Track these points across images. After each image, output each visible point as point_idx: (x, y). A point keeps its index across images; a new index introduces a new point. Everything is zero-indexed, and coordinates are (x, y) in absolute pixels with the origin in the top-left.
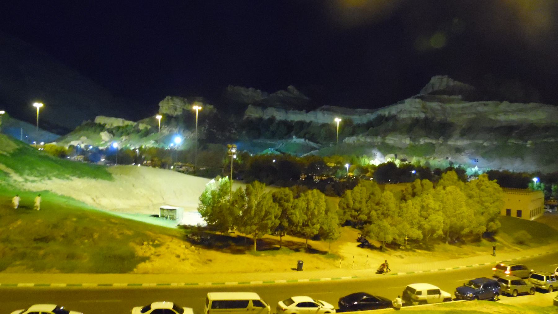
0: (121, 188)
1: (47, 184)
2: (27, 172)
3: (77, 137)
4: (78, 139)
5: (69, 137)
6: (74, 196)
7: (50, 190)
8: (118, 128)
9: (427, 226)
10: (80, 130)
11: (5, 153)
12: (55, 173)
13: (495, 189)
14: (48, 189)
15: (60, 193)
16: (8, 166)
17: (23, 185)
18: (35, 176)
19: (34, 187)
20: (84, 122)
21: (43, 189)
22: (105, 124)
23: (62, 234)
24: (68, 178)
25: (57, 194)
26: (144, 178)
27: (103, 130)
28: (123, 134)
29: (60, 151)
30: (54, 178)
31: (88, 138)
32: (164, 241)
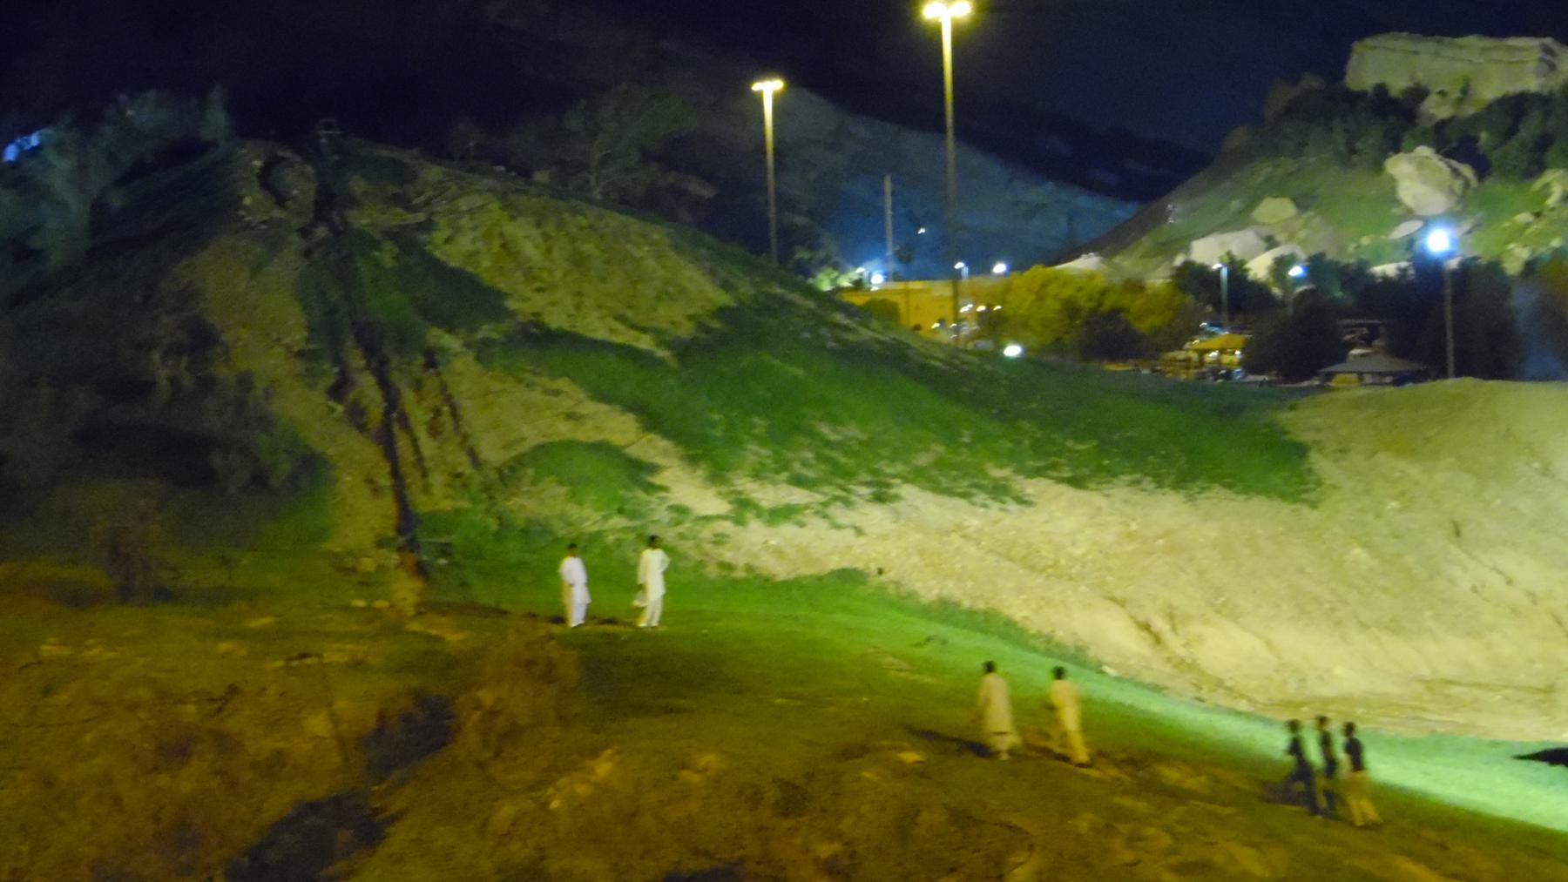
0: (1357, 551)
1: (859, 531)
2: (755, 452)
3: (1235, 204)
4: (1239, 221)
5: (1176, 210)
6: (1017, 609)
7: (873, 567)
8: (1516, 107)
9: (465, 222)
10: (1247, 156)
11: (645, 343)
12: (923, 459)
13: (1484, 49)
14: (860, 565)
15: (928, 589)
16: (652, 421)
17: (720, 539)
18: (798, 481)
19: (779, 552)
20: (1282, 95)
21: (835, 563)
22: (1418, 93)
23: (825, 850)
24: (999, 491)
25: (911, 595)
26: (1546, 471)
27: (1407, 141)
28: (1551, 154)
29: (1093, 312)
30: (908, 491)
31: (1303, 202)
32: (643, 605)
